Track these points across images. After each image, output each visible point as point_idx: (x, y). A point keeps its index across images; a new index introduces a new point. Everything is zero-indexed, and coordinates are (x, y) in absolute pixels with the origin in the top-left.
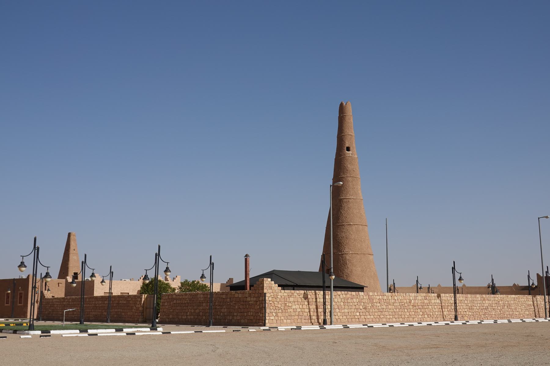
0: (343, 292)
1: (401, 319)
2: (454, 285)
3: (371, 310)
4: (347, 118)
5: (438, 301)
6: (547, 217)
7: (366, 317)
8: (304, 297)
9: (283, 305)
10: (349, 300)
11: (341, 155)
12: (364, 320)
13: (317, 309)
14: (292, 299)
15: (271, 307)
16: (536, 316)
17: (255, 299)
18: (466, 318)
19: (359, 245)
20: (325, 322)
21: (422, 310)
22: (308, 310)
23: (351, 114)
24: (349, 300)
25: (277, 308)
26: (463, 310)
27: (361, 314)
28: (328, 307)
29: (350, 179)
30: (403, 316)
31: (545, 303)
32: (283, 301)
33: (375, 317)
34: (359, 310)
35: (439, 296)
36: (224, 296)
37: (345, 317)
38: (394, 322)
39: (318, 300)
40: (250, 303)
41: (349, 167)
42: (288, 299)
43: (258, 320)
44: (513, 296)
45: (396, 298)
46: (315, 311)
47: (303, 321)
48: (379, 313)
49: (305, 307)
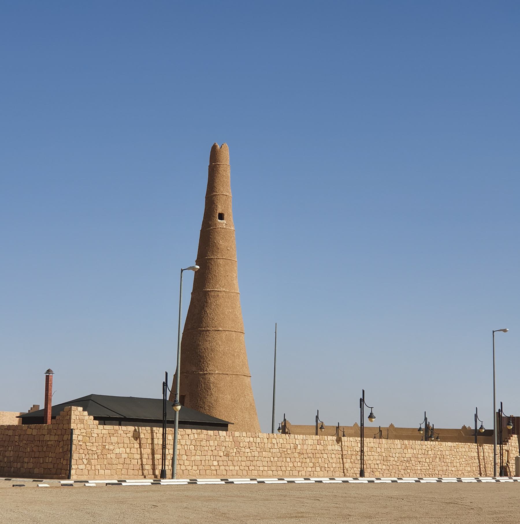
0: (194, 431)
1: (280, 473)
2: (362, 425)
3: (236, 459)
4: (221, 169)
5: (337, 447)
6: (505, 331)
7: (227, 468)
8: (133, 437)
9: (100, 447)
10: (204, 443)
11: (210, 226)
12: (224, 473)
13: (153, 454)
14: (114, 439)
15: (81, 451)
16: (480, 474)
17: (56, 438)
18: (377, 474)
19: (230, 362)
20: (163, 475)
21: (313, 460)
22: (138, 456)
23: (228, 163)
24: (204, 443)
25: (90, 452)
26: (374, 462)
27: (221, 463)
28: (169, 451)
29: (221, 262)
30: (284, 469)
31: (495, 455)
32: (101, 441)
33: (242, 468)
34: (218, 458)
35: (339, 440)
36: (10, 433)
37: (195, 468)
38: (295, 476)
39: (156, 441)
40: (49, 443)
41: (221, 243)
42: (108, 438)
43: (61, 470)
44: (450, 444)
45: (274, 441)
46: (151, 457)
47: (131, 472)
48: (248, 463)
49: (134, 451)
